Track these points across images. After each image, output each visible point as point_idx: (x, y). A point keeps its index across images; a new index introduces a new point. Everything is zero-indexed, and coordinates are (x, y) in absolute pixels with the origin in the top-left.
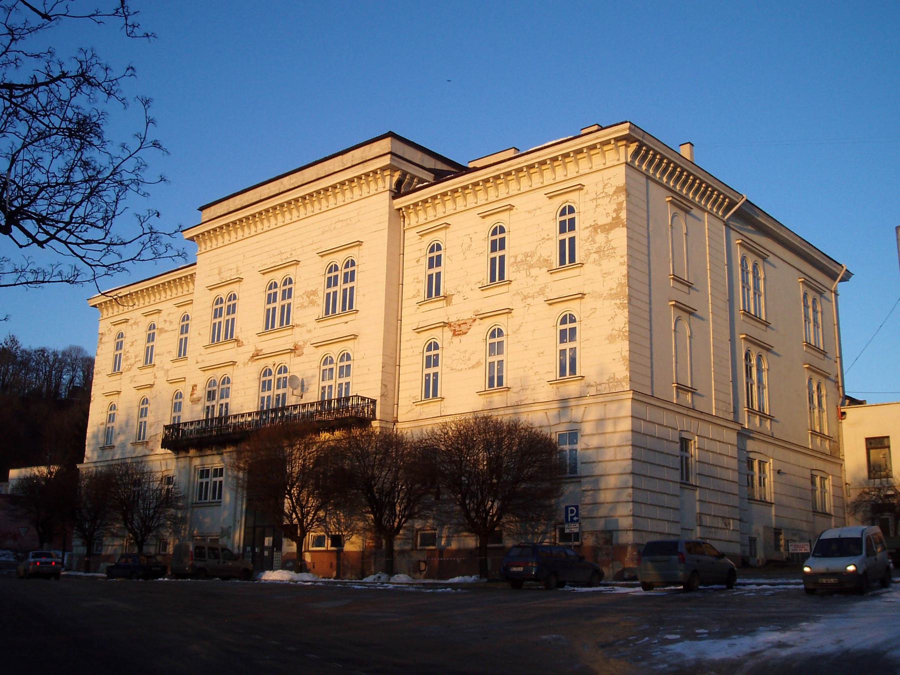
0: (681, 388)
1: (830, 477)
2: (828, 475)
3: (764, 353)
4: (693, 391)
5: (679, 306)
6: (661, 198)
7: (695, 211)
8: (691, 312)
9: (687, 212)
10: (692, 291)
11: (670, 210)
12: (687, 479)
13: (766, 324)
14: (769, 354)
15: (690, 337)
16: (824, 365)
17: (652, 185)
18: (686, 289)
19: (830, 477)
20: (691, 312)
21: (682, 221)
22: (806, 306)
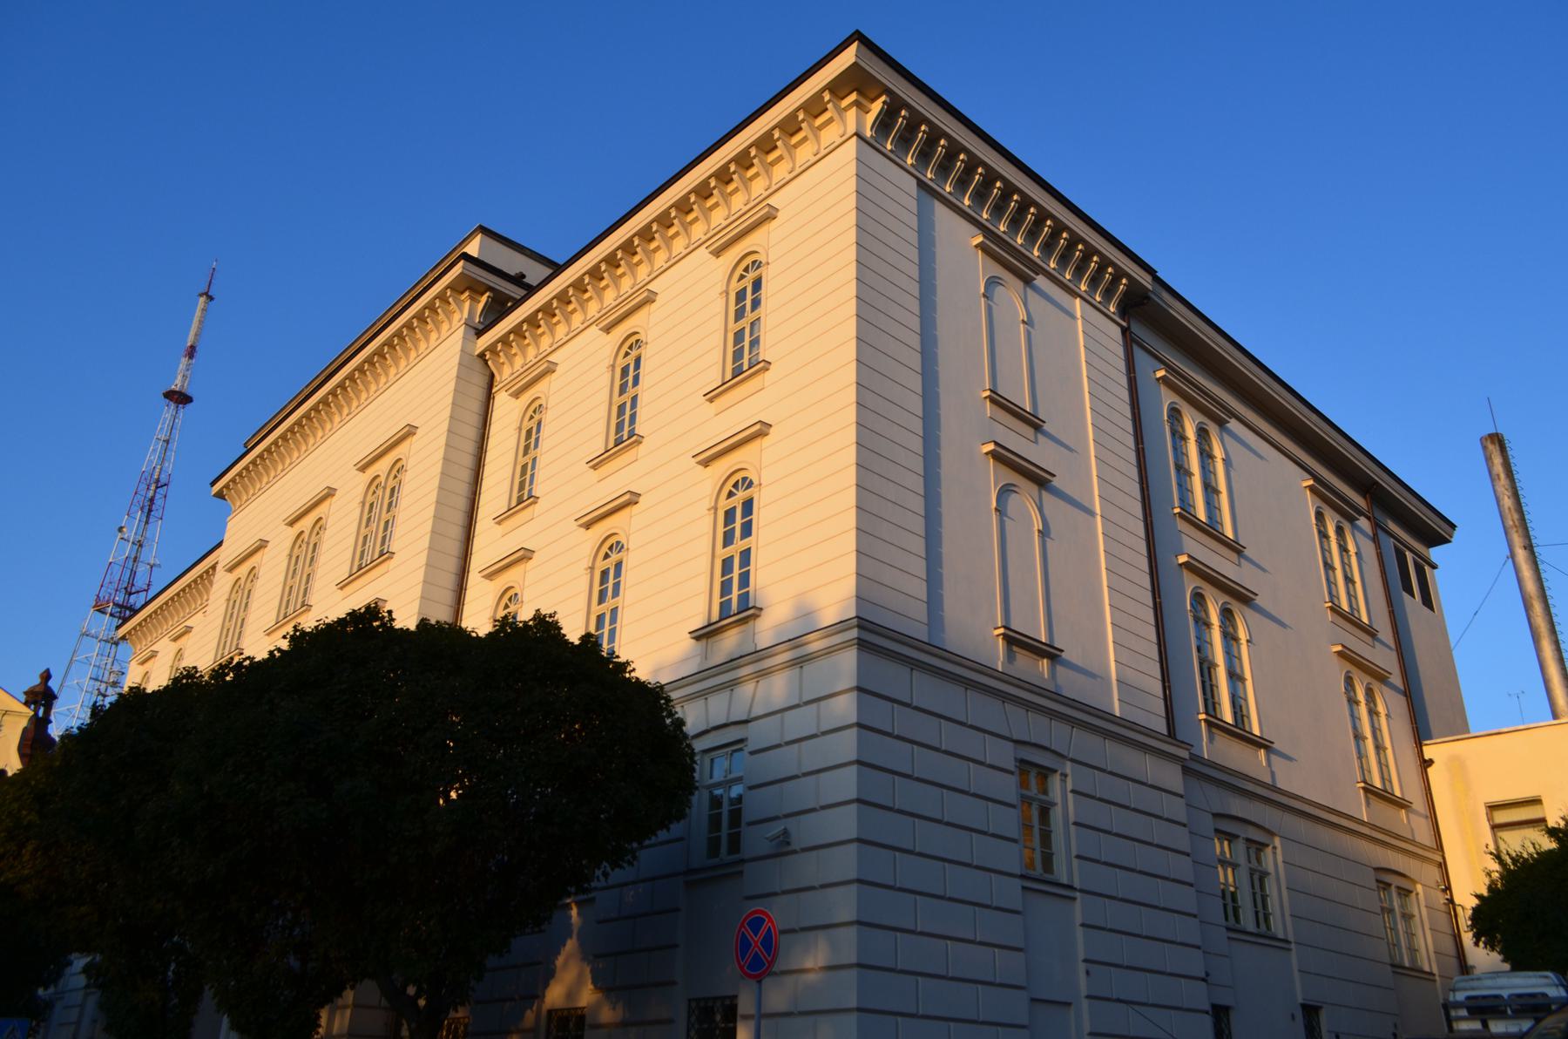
0: (1015, 641)
1: (1277, 841)
2: (1271, 834)
3: (1236, 607)
4: (1050, 653)
5: (1002, 457)
6: (959, 241)
7: (1041, 281)
8: (1040, 480)
9: (1027, 281)
10: (1040, 436)
11: (982, 268)
12: (1237, 920)
13: (1235, 548)
14: (1248, 611)
15: (1044, 533)
16: (1038, 453)
17: (940, 210)
18: (1029, 431)
19: (1277, 841)
20: (1040, 480)
21: (1011, 294)
22: (1323, 535)
